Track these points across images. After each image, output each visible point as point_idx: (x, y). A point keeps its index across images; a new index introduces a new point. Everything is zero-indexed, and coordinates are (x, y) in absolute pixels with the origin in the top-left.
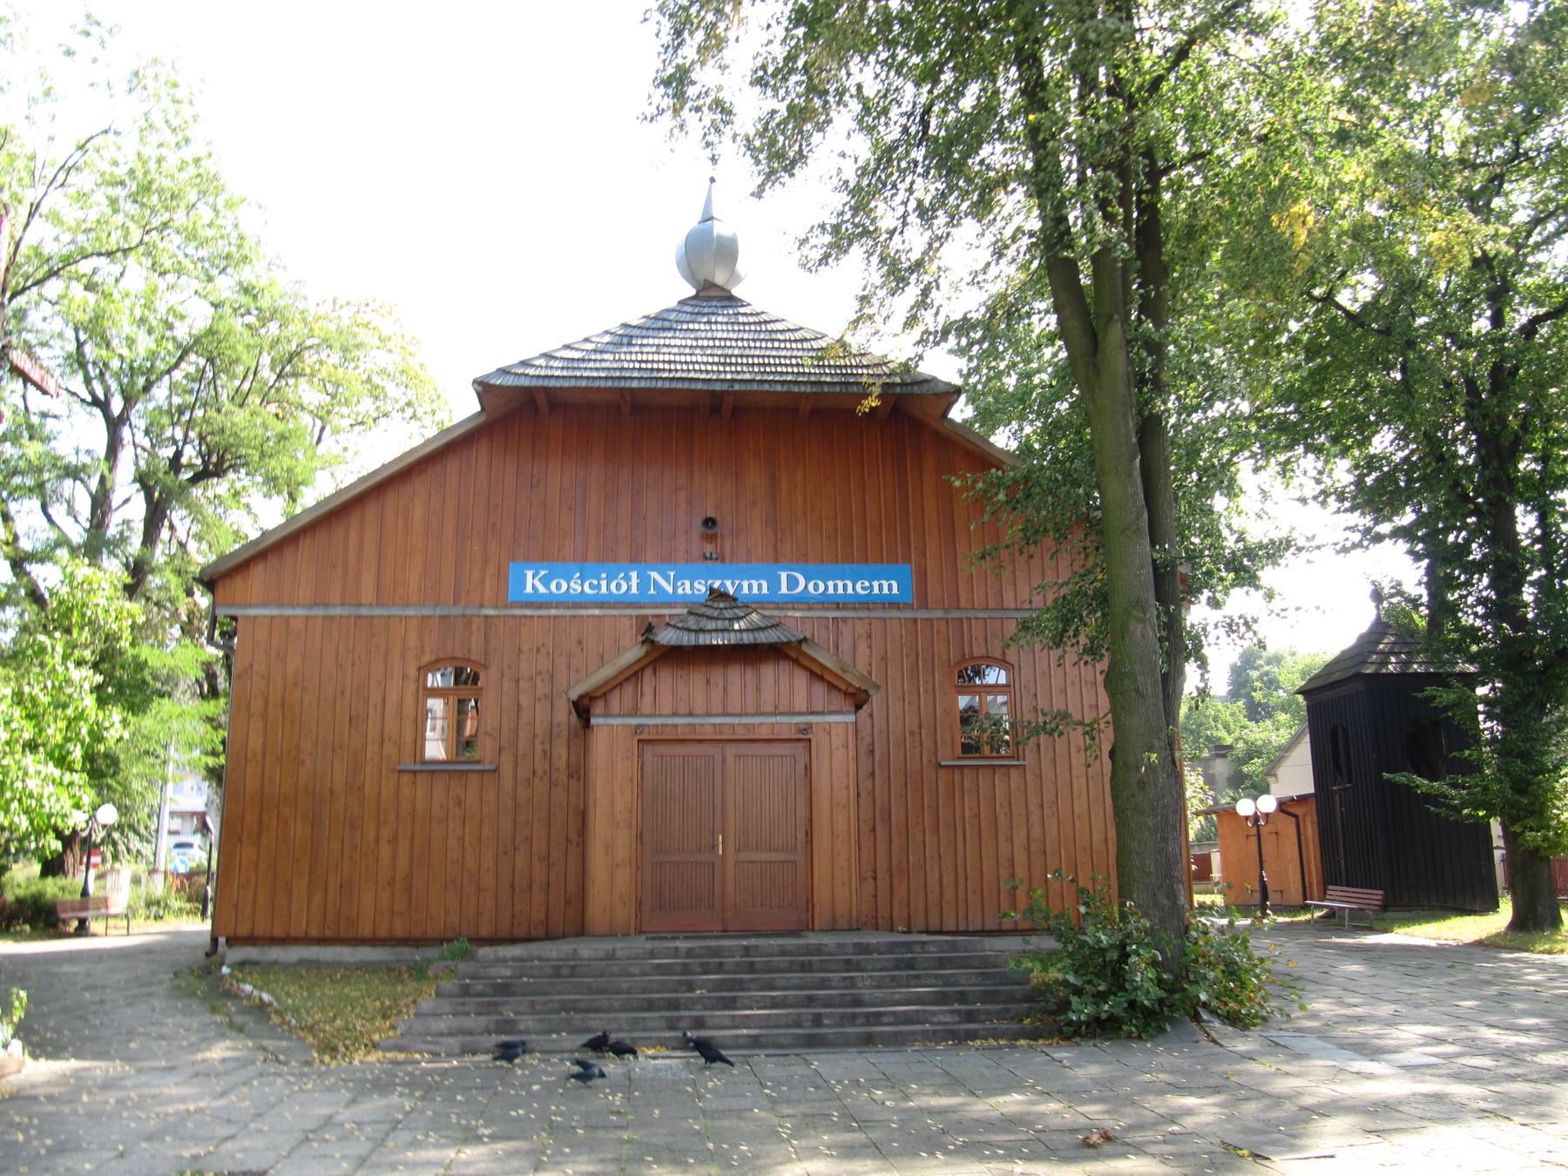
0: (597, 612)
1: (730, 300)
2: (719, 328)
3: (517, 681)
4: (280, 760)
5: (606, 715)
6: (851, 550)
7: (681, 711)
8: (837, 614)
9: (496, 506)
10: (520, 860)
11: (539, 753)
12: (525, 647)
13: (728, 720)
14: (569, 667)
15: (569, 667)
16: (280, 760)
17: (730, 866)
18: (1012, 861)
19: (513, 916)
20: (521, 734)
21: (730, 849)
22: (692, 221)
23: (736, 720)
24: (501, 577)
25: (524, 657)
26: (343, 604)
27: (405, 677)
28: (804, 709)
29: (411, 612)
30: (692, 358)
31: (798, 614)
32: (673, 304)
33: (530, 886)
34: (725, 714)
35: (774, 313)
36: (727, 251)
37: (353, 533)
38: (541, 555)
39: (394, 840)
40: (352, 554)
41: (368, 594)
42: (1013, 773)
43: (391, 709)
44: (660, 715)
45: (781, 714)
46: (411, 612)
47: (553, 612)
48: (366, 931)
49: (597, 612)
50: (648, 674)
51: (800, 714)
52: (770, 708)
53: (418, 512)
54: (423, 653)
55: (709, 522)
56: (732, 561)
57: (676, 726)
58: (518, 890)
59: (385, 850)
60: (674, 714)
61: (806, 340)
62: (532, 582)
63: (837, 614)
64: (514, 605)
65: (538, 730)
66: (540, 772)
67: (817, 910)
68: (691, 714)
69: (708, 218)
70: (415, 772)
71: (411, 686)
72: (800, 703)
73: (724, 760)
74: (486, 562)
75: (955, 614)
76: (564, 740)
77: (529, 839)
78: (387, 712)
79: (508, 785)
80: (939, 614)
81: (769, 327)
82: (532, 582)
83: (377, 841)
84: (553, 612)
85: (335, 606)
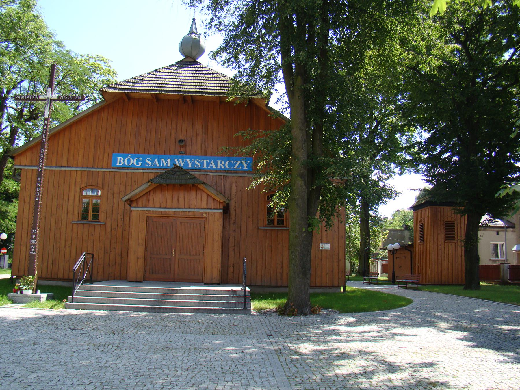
0: (141, 171)
2: (189, 72)
3: (113, 194)
5: (137, 207)
7: (186, 207)
8: (225, 174)
11: (120, 220)
12: (116, 183)
13: (178, 210)
17: (177, 260)
18: (282, 263)
20: (114, 212)
21: (177, 255)
22: (185, 32)
23: (181, 210)
24: (109, 159)
25: (116, 186)
26: (56, 166)
28: (205, 207)
29: (79, 169)
30: (185, 81)
31: (211, 174)
32: (166, 65)
37: (60, 142)
38: (123, 151)
39: (71, 246)
40: (60, 149)
41: (65, 163)
43: (71, 202)
47: (126, 171)
48: (61, 276)
49: (141, 171)
50: (152, 193)
51: (203, 209)
53: (82, 135)
54: (81, 183)
55: (181, 141)
58: (111, 265)
59: (68, 249)
60: (160, 207)
61: (218, 77)
62: (121, 161)
63: (225, 174)
64: (113, 168)
65: (120, 211)
66: (119, 226)
68: (166, 208)
70: (78, 224)
71: (77, 195)
72: (204, 205)
74: (104, 153)
78: (69, 203)
79: (109, 230)
82: (121, 161)
84: (126, 171)
85: (53, 167)
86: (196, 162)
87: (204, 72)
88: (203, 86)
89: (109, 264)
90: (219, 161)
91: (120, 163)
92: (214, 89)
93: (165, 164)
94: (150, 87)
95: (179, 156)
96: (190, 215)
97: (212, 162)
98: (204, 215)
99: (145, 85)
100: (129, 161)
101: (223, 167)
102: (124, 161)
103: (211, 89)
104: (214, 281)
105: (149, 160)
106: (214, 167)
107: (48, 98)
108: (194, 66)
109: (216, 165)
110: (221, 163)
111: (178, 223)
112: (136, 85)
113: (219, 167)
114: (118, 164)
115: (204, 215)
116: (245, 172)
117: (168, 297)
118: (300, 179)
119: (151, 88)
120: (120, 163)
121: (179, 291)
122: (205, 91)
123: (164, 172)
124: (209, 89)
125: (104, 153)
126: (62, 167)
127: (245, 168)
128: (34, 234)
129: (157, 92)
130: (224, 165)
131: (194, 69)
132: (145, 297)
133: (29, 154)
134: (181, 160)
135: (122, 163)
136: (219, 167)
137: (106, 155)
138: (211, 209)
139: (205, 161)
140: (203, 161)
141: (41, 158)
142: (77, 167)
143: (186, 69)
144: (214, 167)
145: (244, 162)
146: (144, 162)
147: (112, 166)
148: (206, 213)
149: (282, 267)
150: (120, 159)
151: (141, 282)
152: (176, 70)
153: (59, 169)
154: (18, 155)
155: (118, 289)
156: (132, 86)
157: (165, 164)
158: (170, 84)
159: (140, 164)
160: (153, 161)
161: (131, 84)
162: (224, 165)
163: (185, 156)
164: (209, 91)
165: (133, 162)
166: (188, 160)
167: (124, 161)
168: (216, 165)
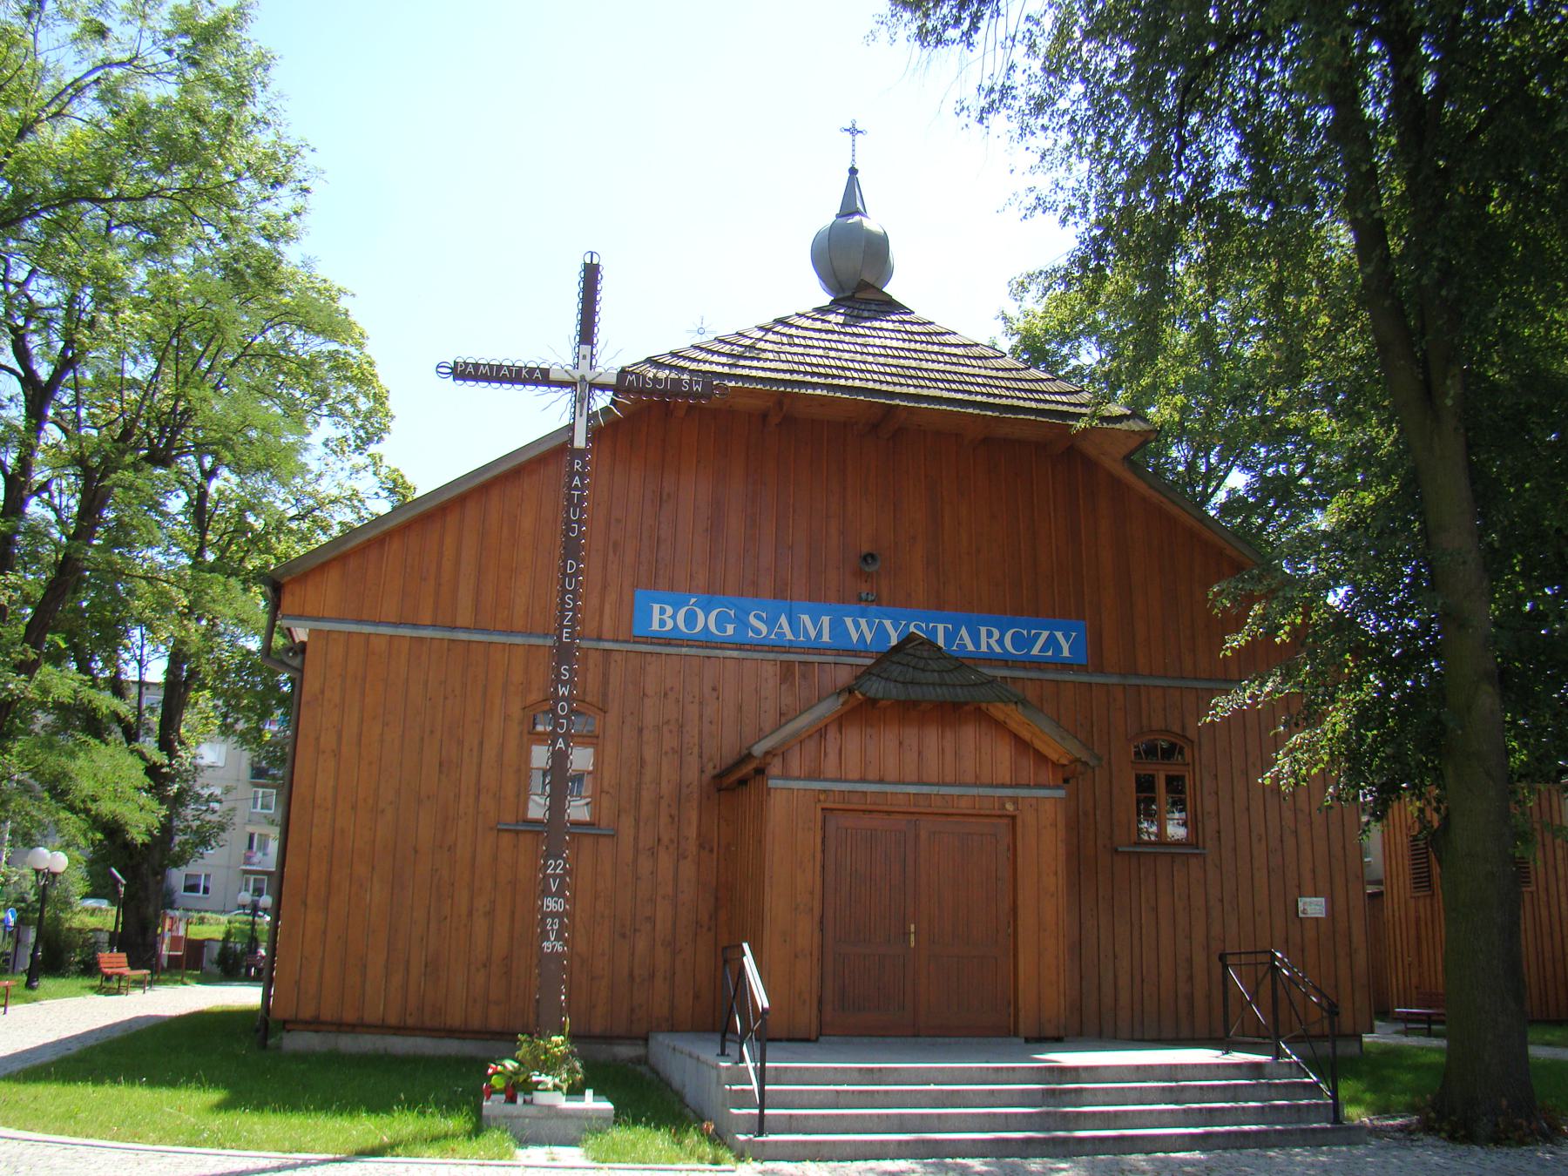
1: (890, 306)
2: (882, 334)
3: (641, 731)
4: (354, 807)
5: (785, 776)
6: (1019, 601)
7: (870, 777)
9: (618, 521)
10: (642, 945)
11: (664, 819)
13: (925, 790)
14: (701, 716)
15: (701, 716)
16: (354, 807)
18: (1190, 961)
19: (632, 1010)
22: (826, 214)
23: (934, 790)
27: (507, 717)
29: (518, 640)
33: (652, 976)
34: (920, 782)
35: (942, 323)
36: (876, 250)
39: (490, 914)
41: (464, 618)
42: (1193, 861)
44: (846, 781)
45: (982, 785)
46: (518, 640)
48: (455, 1019)
49: (735, 654)
50: (832, 734)
51: (1003, 786)
52: (970, 778)
55: (869, 558)
56: (888, 605)
57: (865, 793)
60: (863, 780)
61: (986, 358)
62: (663, 617)
66: (665, 840)
67: (1022, 1014)
68: (881, 781)
69: (851, 205)
70: (517, 832)
72: (1004, 774)
73: (917, 836)
74: (604, 587)
75: (1133, 681)
76: (695, 804)
77: (651, 919)
80: (1114, 680)
81: (942, 339)
82: (663, 617)
83: (470, 914)
84: (684, 650)
85: (425, 626)
86: (764, 629)
87: (935, 339)
88: (954, 382)
89: (631, 976)
90: (983, 630)
91: (662, 623)
92: (995, 396)
93: (813, 634)
94: (792, 372)
95: (857, 608)
96: (964, 806)
97: (963, 632)
98: (1010, 807)
99: (768, 365)
100: (691, 619)
101: (998, 649)
102: (674, 617)
103: (983, 394)
104: (1051, 1032)
105: (758, 617)
106: (971, 647)
107: (583, 378)
108: (894, 318)
109: (977, 643)
110: (990, 635)
111: (923, 835)
112: (742, 362)
113: (984, 648)
114: (655, 626)
115: (1010, 807)
116: (1065, 666)
117: (1066, 1098)
118: (1490, 689)
119: (795, 377)
120: (662, 623)
121: (1083, 1075)
122: (966, 397)
123: (869, 662)
124: (977, 393)
125: (604, 587)
126: (454, 628)
127: (1066, 653)
128: (555, 876)
129: (818, 392)
130: (1000, 642)
131: (898, 326)
132: (991, 1100)
133: (334, 575)
134: (863, 622)
135: (670, 625)
136: (984, 648)
137: (612, 596)
138: (1028, 786)
139: (941, 627)
140: (935, 628)
141: (566, 592)
142: (512, 633)
143: (877, 324)
144: (971, 647)
145: (1059, 635)
146: (742, 624)
147: (636, 632)
148: (1015, 800)
149: (1191, 978)
150: (663, 612)
151: (807, 1040)
152: (843, 325)
153: (447, 635)
154: (294, 580)
155: (876, 1076)
156: (730, 366)
157: (813, 634)
158: (849, 369)
159: (730, 629)
160: (771, 622)
161: (724, 360)
162: (1000, 642)
163: (873, 608)
164: (979, 398)
165: (707, 621)
166: (888, 623)
167: (674, 617)
168: (976, 640)
